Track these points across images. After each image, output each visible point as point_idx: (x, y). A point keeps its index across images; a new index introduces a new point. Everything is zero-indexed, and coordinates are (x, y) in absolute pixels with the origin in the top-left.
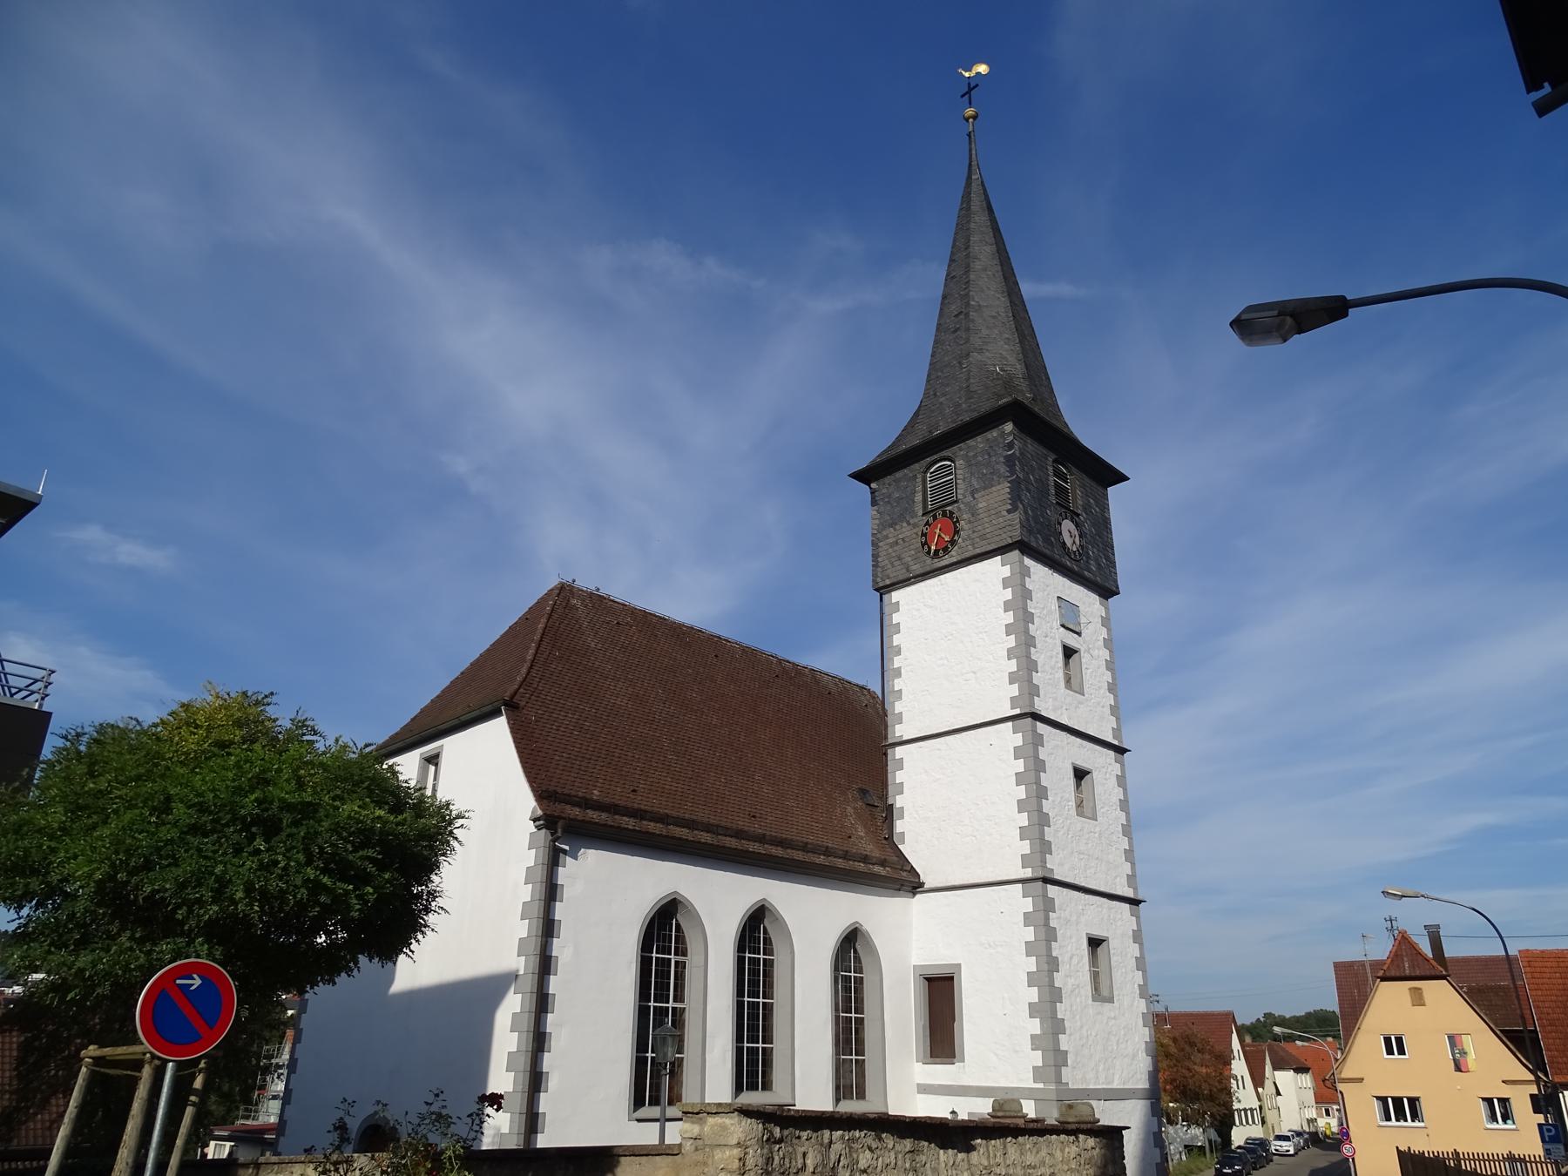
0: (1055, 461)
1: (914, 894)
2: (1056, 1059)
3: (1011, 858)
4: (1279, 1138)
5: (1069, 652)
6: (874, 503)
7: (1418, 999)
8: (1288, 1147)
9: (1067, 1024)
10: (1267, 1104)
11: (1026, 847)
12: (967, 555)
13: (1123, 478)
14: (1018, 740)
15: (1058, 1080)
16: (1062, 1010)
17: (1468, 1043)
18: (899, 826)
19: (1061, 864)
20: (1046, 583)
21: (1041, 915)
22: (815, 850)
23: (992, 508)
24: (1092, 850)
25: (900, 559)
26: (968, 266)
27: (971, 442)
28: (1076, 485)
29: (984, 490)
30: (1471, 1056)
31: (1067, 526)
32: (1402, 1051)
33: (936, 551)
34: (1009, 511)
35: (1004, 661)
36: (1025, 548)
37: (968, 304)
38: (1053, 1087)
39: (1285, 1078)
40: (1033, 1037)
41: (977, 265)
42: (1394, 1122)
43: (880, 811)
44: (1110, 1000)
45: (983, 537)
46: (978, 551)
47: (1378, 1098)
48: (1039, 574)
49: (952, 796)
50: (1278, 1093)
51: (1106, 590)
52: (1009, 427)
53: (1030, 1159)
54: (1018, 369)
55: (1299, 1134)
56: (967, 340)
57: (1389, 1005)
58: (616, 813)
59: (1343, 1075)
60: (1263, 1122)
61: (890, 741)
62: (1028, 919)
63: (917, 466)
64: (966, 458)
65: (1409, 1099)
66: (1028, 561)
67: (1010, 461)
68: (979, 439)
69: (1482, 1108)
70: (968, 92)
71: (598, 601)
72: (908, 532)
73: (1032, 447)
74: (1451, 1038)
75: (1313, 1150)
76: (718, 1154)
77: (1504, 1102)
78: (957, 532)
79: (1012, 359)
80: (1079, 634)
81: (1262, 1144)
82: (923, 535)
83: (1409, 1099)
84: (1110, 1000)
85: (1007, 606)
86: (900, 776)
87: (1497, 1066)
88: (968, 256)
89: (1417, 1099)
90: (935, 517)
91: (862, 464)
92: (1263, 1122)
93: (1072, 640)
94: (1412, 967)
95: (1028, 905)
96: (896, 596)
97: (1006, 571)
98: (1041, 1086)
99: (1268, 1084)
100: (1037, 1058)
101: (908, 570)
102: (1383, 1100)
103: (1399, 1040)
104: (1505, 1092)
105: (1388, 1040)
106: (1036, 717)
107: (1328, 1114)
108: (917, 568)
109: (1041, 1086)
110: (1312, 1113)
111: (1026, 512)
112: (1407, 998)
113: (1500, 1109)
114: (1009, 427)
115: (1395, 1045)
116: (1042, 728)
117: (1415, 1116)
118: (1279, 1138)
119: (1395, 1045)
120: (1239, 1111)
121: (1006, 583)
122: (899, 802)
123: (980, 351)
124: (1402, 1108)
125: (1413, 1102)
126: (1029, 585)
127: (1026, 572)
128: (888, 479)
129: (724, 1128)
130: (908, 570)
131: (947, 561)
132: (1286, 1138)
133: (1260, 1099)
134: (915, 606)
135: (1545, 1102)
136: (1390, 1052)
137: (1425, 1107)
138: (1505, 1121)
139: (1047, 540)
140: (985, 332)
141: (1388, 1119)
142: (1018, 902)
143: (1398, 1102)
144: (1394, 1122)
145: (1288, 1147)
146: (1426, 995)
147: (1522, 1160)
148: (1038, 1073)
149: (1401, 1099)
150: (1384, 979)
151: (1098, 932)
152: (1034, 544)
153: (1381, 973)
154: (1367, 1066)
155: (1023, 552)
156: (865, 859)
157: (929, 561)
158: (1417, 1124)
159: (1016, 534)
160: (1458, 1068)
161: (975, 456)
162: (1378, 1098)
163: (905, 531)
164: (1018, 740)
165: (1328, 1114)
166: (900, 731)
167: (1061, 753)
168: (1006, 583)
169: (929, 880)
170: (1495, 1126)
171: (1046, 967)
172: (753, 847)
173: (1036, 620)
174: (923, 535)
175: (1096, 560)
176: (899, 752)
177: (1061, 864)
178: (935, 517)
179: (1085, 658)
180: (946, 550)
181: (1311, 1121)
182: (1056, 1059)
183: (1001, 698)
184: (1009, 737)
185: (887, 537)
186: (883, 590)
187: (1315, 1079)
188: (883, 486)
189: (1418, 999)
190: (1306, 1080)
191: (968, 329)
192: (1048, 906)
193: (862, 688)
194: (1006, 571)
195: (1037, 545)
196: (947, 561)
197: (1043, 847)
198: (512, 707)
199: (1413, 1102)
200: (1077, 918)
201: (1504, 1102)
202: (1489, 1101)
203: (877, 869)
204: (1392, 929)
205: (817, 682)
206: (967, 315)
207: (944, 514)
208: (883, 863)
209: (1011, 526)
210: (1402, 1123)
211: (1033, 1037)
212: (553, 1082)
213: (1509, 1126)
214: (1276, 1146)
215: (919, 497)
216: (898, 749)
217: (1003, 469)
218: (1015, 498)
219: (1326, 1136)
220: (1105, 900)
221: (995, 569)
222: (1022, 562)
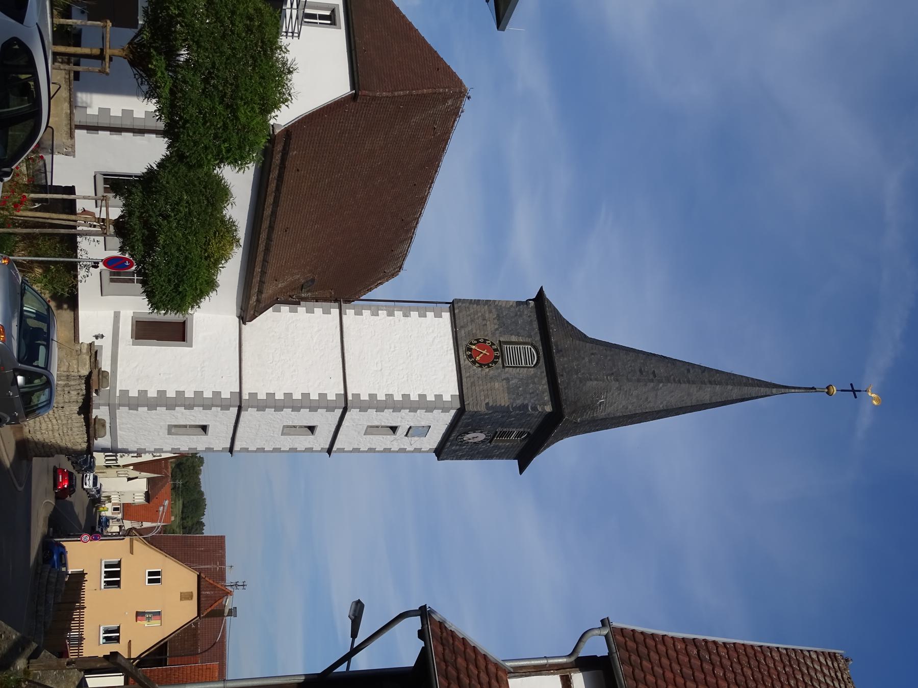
0: (529, 433)
1: (239, 317)
2: (134, 404)
3: (257, 385)
4: (95, 478)
5: (394, 429)
6: (519, 303)
7: (185, 596)
8: (89, 485)
9: (154, 412)
10: (121, 471)
11: (262, 396)
12: (463, 372)
13: (521, 471)
14: (331, 397)
15: (120, 405)
16: (161, 410)
17: (155, 623)
18: (285, 309)
19: (251, 415)
20: (440, 422)
21: (219, 403)
22: (264, 267)
23: (496, 392)
24: (259, 431)
25: (472, 321)
26: (694, 383)
27: (545, 381)
28: (514, 439)
29: (518, 381)
30: (146, 623)
31: (481, 436)
32: (150, 581)
33: (470, 349)
34: (487, 404)
35: (385, 391)
36: (461, 412)
37: (661, 381)
38: (117, 402)
39: (141, 485)
40: (146, 391)
41: (693, 389)
42: (104, 570)
43: (292, 298)
44: (169, 433)
45: (473, 384)
46: (464, 380)
47: (120, 562)
48: (448, 417)
49: (299, 348)
50: (129, 479)
51: (440, 452)
52: (549, 409)
53: (75, 429)
54: (601, 414)
55: (99, 491)
56: (629, 380)
57: (181, 578)
58: (280, 168)
59: (135, 542)
60: (107, 467)
61: (343, 305)
62: (217, 394)
63: (538, 338)
64: (535, 376)
65: (119, 581)
66: (453, 412)
67: (524, 407)
68: (546, 387)
69: (114, 626)
70: (853, 391)
71: (455, 113)
72: (490, 330)
73: (536, 422)
74: (159, 614)
75: (87, 500)
76: (75, 362)
77: (117, 639)
78: (481, 366)
79: (609, 410)
80: (406, 435)
81: (91, 467)
82: (485, 340)
83: (119, 581)
84: (169, 433)
85: (422, 397)
86: (318, 311)
87: (140, 639)
88: (703, 383)
89: (119, 587)
90: (496, 350)
91: (548, 294)
92: (107, 467)
93: (401, 432)
94: (207, 596)
95: (226, 395)
96: (446, 316)
97: (447, 398)
98: (118, 394)
99: (136, 474)
100: (133, 393)
101: (462, 327)
102: (118, 565)
103: (158, 581)
104: (124, 640)
105: (158, 573)
106: (345, 410)
107: (115, 509)
108: (462, 333)
109: (118, 394)
110: (115, 499)
111: (486, 414)
112: (186, 589)
113: (112, 635)
114: (549, 409)
115: (155, 577)
116: (339, 412)
117: (108, 584)
118: (95, 478)
119: (155, 577)
120: (116, 456)
121: (439, 397)
122: (301, 309)
123: (619, 389)
124: (113, 576)
125: (117, 584)
126: (435, 411)
127: (445, 410)
128: (534, 316)
129: (85, 364)
130: (462, 327)
131: (463, 357)
132: (95, 484)
133: (124, 466)
134: (439, 327)
135: (111, 664)
136: (150, 574)
137: (113, 591)
138: (105, 638)
139: (468, 425)
140: (635, 393)
141: (106, 566)
142: (228, 389)
143: (117, 574)
144: (104, 570)
145: (89, 485)
146: (186, 603)
147: (80, 645)
148: (125, 393)
149: (119, 576)
150: (199, 577)
151: (210, 430)
152: (464, 417)
153: (202, 575)
154: (140, 559)
155: (458, 410)
156: (260, 292)
157: (464, 343)
158: (103, 584)
159: (470, 408)
160: (138, 614)
161: (534, 383)
162: (120, 562)
163: (491, 327)
164: (331, 397)
165: (115, 509)
166: (350, 314)
167: (325, 421)
168: (439, 397)
169: (248, 327)
170: (102, 632)
171: (187, 403)
172: (263, 236)
173: (412, 414)
174: (485, 340)
175: (459, 450)
176: (335, 312)
177: (251, 415)
178: (496, 350)
179: (391, 437)
180: (470, 357)
181: (109, 499)
182: (134, 404)
183: (359, 388)
184: (333, 391)
185: (490, 312)
186: (453, 307)
187: (140, 506)
188: (530, 313)
189: (185, 596)
190: (140, 499)
191: (639, 381)
192: (225, 407)
193: (401, 267)
194: (447, 398)
195: (462, 421)
196: (463, 357)
197: (261, 406)
198: (353, 98)
199: (117, 584)
200: (220, 423)
201: (117, 639)
202: (117, 630)
203: (254, 298)
204: (236, 585)
205: (402, 242)
206: (652, 381)
207: (497, 357)
208: (258, 301)
209: (476, 405)
210: (103, 575)
211: (146, 391)
212: (116, 137)
213: (102, 641)
214: (90, 477)
215: (514, 339)
216: (338, 311)
217: (519, 402)
218: (495, 409)
219: (97, 508)
220: (231, 435)
221: (449, 389)
222: (452, 408)
